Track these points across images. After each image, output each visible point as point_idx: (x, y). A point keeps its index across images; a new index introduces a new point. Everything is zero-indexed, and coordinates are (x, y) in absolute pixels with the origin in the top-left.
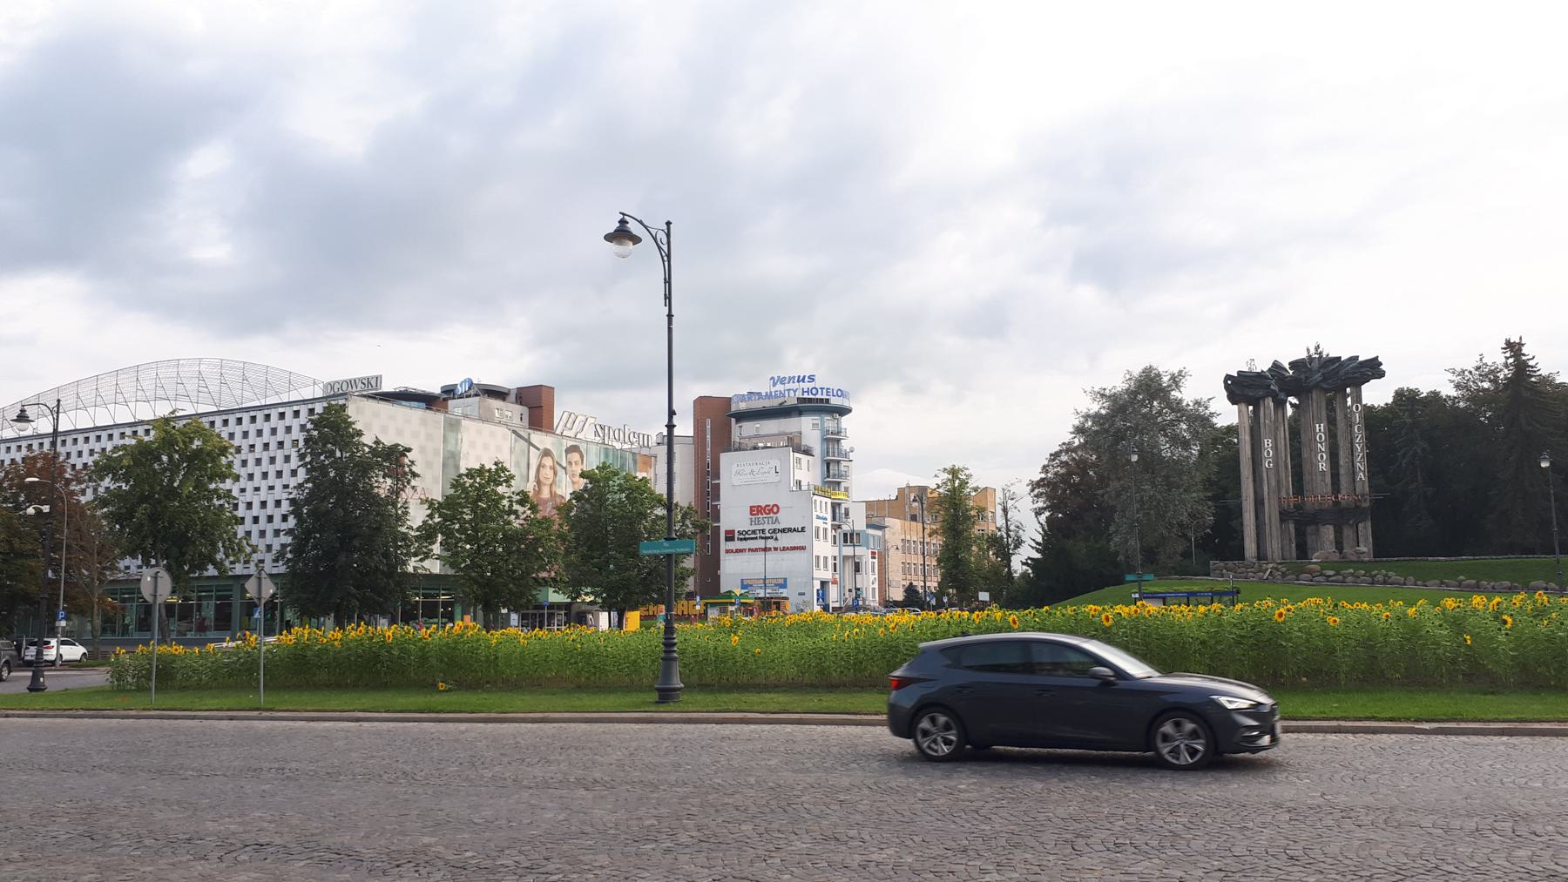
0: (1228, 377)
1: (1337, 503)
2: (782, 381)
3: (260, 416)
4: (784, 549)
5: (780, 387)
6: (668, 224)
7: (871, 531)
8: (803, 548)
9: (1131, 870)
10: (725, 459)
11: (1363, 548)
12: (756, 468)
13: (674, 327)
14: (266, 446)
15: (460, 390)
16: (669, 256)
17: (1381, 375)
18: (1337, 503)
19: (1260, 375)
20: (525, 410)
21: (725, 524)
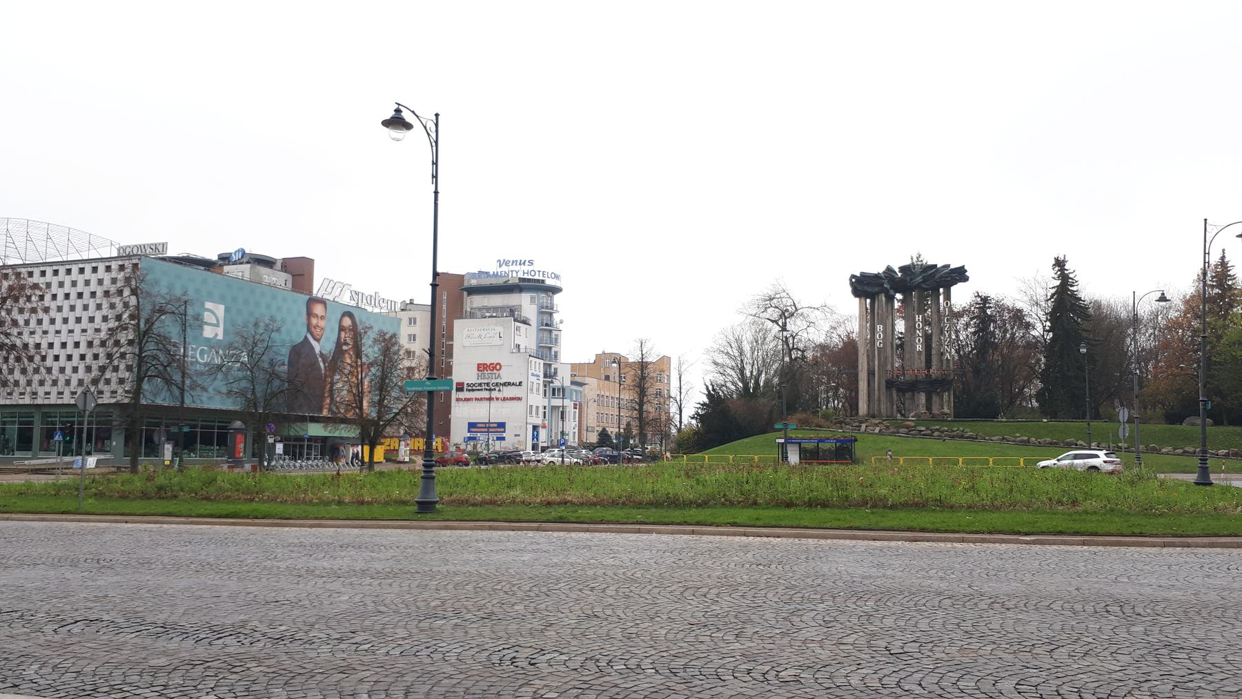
0: (853, 276)
1: (928, 376)
2: (507, 263)
3: (62, 270)
4: (504, 399)
5: (504, 268)
6: (437, 115)
7: (574, 387)
8: (519, 399)
9: (844, 641)
10: (458, 324)
11: (946, 410)
12: (483, 333)
13: (439, 202)
14: (67, 296)
15: (234, 258)
16: (436, 142)
17: (966, 279)
18: (928, 376)
19: (877, 276)
20: (289, 277)
21: (456, 377)
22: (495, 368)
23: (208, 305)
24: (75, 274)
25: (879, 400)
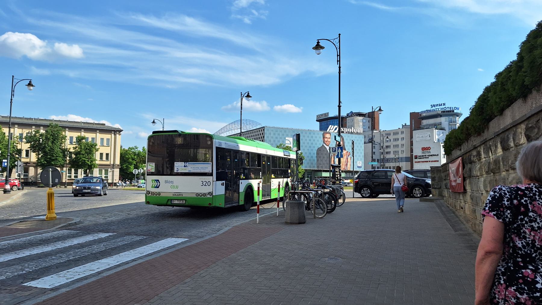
2: (434, 106)
4: (432, 161)
5: (434, 108)
6: (340, 34)
12: (423, 135)
22: (428, 149)
23: (287, 138)
24: (312, 134)
25: (259, 195)
